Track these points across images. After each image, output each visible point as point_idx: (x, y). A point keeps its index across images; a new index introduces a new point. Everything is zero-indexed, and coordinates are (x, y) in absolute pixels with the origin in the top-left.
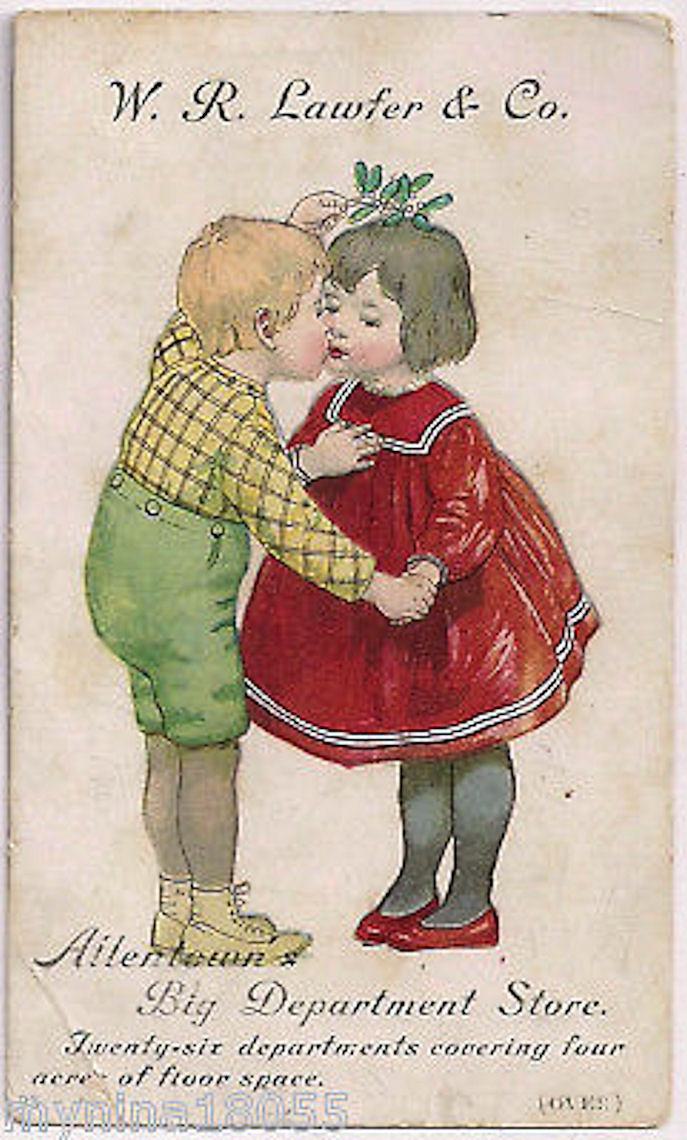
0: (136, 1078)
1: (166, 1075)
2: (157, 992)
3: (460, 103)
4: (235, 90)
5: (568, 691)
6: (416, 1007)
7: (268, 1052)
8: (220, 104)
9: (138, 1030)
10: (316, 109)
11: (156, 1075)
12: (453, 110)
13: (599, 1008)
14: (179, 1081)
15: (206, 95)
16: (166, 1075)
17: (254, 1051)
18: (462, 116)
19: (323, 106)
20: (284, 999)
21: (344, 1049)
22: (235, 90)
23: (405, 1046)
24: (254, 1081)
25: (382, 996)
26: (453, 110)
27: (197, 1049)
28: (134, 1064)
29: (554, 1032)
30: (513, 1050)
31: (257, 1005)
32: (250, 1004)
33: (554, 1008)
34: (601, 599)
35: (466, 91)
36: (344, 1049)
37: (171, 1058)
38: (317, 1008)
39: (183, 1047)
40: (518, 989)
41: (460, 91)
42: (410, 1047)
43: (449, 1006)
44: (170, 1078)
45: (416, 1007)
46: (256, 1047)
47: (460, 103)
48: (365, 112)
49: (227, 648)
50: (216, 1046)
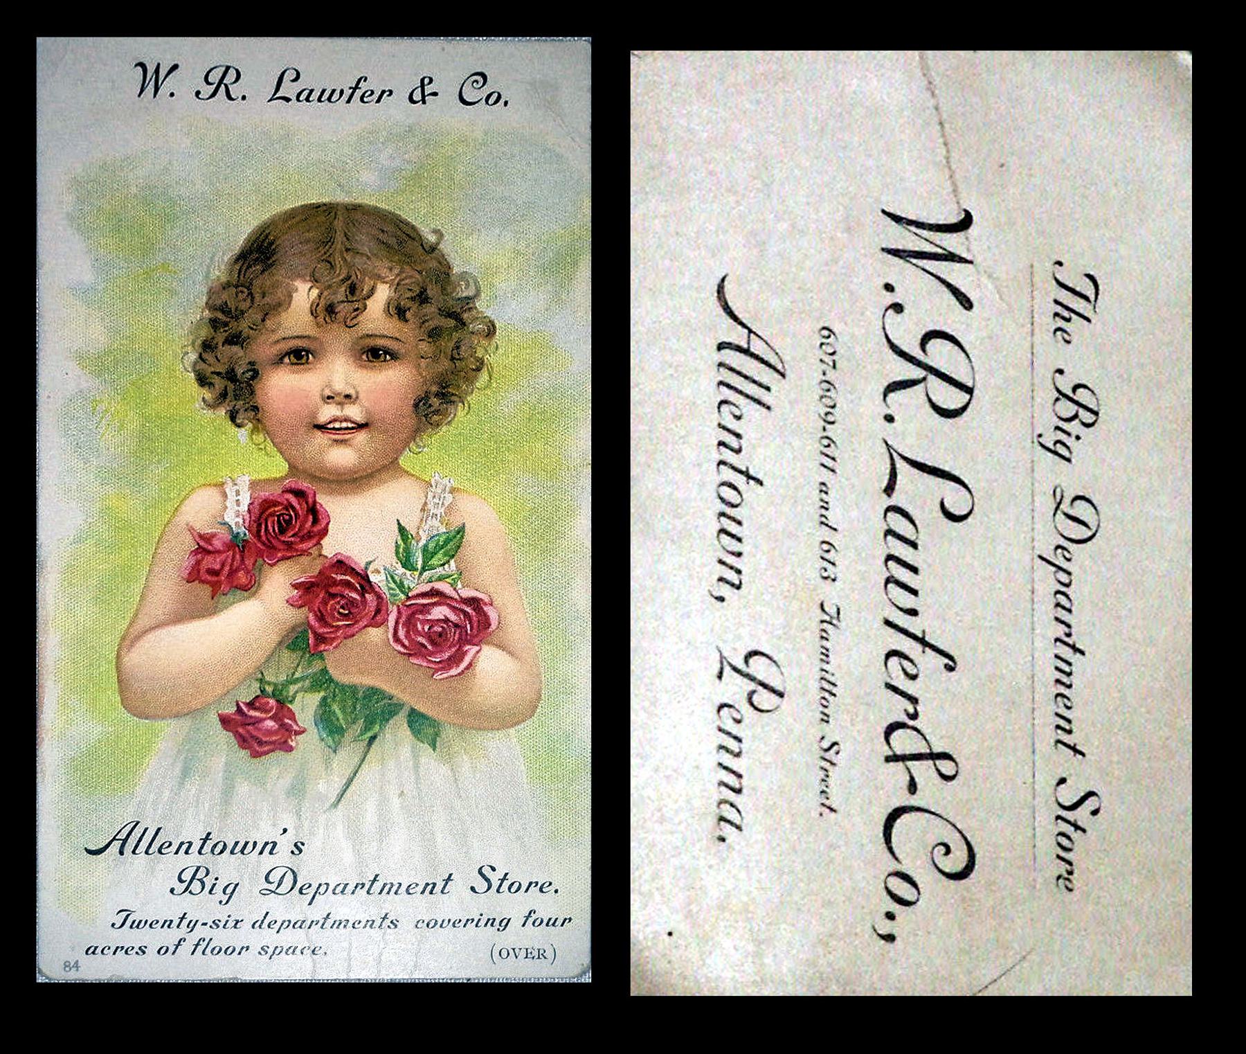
0: (172, 949)
1: (197, 945)
2: (187, 876)
3: (918, 757)
4: (238, 75)
5: (366, 626)
6: (403, 888)
7: (277, 926)
8: (226, 86)
9: (172, 908)
10: (306, 93)
11: (187, 947)
12: (417, 96)
13: (552, 888)
14: (208, 950)
15: (215, 77)
16: (197, 945)
17: (265, 925)
18: (424, 102)
19: (312, 91)
20: (295, 882)
21: (338, 924)
22: (238, 75)
23: (387, 922)
24: (270, 951)
25: (375, 880)
26: (417, 96)
27: (221, 924)
28: (170, 937)
29: (513, 906)
30: (482, 923)
31: (272, 887)
32: (1067, 501)
33: (515, 888)
34: (1187, 722)
35: (426, 81)
36: (338, 924)
37: (200, 932)
38: (322, 889)
39: (210, 923)
40: (487, 871)
41: (422, 80)
42: (392, 922)
43: (430, 887)
44: (200, 949)
45: (403, 888)
46: (266, 922)
47: (918, 757)
48: (345, 97)
49: (924, 632)
50: (237, 922)
